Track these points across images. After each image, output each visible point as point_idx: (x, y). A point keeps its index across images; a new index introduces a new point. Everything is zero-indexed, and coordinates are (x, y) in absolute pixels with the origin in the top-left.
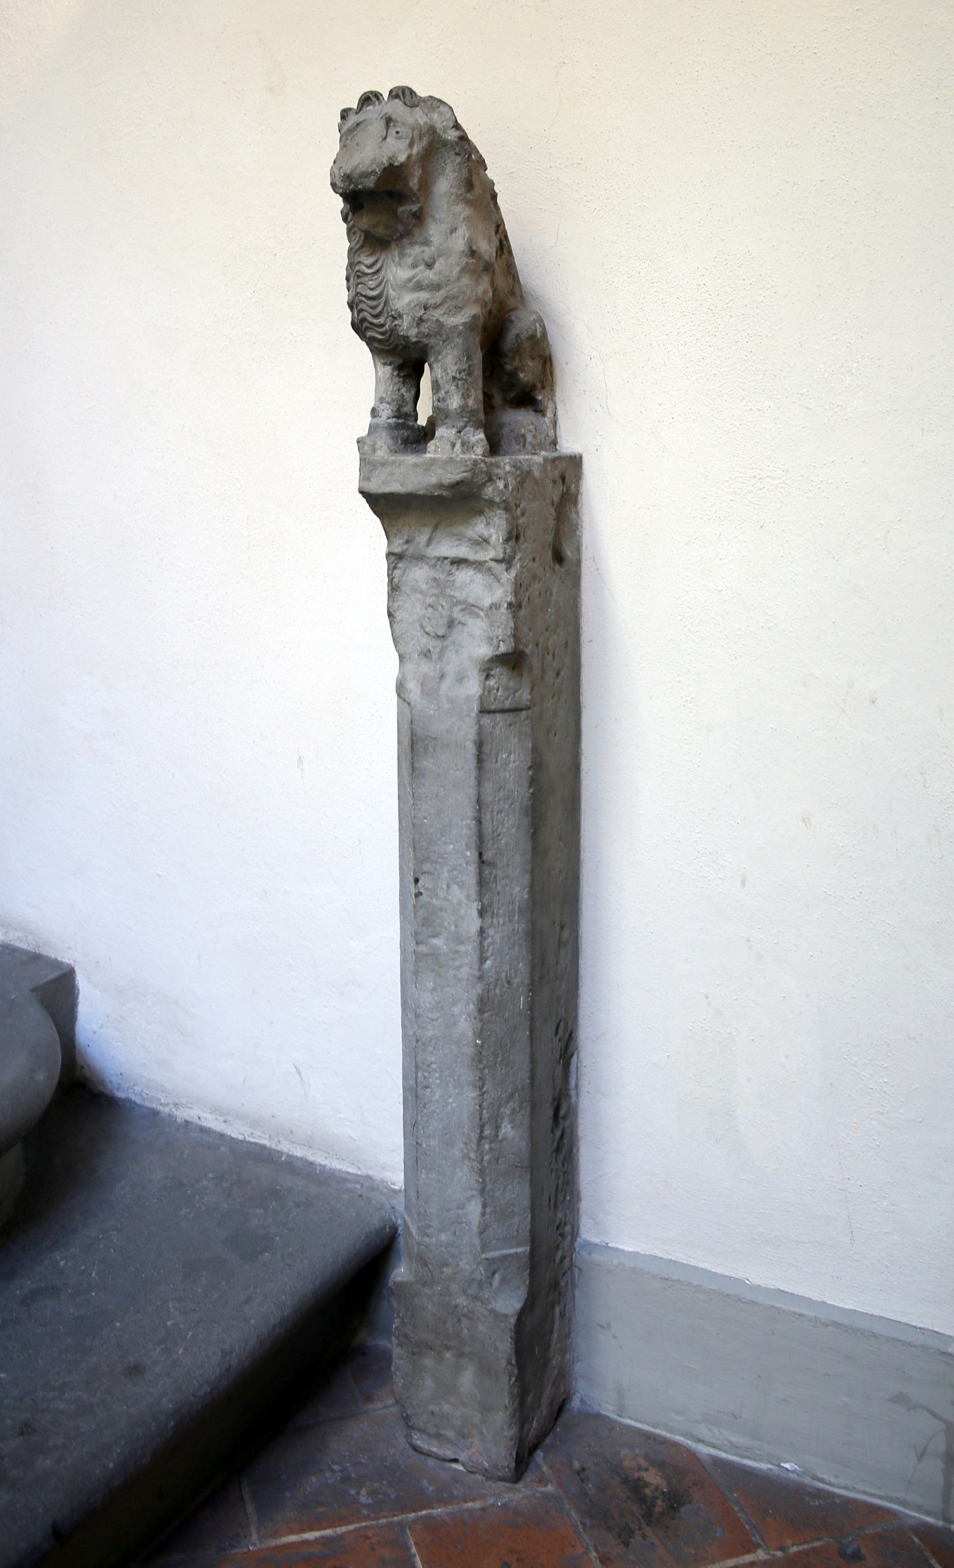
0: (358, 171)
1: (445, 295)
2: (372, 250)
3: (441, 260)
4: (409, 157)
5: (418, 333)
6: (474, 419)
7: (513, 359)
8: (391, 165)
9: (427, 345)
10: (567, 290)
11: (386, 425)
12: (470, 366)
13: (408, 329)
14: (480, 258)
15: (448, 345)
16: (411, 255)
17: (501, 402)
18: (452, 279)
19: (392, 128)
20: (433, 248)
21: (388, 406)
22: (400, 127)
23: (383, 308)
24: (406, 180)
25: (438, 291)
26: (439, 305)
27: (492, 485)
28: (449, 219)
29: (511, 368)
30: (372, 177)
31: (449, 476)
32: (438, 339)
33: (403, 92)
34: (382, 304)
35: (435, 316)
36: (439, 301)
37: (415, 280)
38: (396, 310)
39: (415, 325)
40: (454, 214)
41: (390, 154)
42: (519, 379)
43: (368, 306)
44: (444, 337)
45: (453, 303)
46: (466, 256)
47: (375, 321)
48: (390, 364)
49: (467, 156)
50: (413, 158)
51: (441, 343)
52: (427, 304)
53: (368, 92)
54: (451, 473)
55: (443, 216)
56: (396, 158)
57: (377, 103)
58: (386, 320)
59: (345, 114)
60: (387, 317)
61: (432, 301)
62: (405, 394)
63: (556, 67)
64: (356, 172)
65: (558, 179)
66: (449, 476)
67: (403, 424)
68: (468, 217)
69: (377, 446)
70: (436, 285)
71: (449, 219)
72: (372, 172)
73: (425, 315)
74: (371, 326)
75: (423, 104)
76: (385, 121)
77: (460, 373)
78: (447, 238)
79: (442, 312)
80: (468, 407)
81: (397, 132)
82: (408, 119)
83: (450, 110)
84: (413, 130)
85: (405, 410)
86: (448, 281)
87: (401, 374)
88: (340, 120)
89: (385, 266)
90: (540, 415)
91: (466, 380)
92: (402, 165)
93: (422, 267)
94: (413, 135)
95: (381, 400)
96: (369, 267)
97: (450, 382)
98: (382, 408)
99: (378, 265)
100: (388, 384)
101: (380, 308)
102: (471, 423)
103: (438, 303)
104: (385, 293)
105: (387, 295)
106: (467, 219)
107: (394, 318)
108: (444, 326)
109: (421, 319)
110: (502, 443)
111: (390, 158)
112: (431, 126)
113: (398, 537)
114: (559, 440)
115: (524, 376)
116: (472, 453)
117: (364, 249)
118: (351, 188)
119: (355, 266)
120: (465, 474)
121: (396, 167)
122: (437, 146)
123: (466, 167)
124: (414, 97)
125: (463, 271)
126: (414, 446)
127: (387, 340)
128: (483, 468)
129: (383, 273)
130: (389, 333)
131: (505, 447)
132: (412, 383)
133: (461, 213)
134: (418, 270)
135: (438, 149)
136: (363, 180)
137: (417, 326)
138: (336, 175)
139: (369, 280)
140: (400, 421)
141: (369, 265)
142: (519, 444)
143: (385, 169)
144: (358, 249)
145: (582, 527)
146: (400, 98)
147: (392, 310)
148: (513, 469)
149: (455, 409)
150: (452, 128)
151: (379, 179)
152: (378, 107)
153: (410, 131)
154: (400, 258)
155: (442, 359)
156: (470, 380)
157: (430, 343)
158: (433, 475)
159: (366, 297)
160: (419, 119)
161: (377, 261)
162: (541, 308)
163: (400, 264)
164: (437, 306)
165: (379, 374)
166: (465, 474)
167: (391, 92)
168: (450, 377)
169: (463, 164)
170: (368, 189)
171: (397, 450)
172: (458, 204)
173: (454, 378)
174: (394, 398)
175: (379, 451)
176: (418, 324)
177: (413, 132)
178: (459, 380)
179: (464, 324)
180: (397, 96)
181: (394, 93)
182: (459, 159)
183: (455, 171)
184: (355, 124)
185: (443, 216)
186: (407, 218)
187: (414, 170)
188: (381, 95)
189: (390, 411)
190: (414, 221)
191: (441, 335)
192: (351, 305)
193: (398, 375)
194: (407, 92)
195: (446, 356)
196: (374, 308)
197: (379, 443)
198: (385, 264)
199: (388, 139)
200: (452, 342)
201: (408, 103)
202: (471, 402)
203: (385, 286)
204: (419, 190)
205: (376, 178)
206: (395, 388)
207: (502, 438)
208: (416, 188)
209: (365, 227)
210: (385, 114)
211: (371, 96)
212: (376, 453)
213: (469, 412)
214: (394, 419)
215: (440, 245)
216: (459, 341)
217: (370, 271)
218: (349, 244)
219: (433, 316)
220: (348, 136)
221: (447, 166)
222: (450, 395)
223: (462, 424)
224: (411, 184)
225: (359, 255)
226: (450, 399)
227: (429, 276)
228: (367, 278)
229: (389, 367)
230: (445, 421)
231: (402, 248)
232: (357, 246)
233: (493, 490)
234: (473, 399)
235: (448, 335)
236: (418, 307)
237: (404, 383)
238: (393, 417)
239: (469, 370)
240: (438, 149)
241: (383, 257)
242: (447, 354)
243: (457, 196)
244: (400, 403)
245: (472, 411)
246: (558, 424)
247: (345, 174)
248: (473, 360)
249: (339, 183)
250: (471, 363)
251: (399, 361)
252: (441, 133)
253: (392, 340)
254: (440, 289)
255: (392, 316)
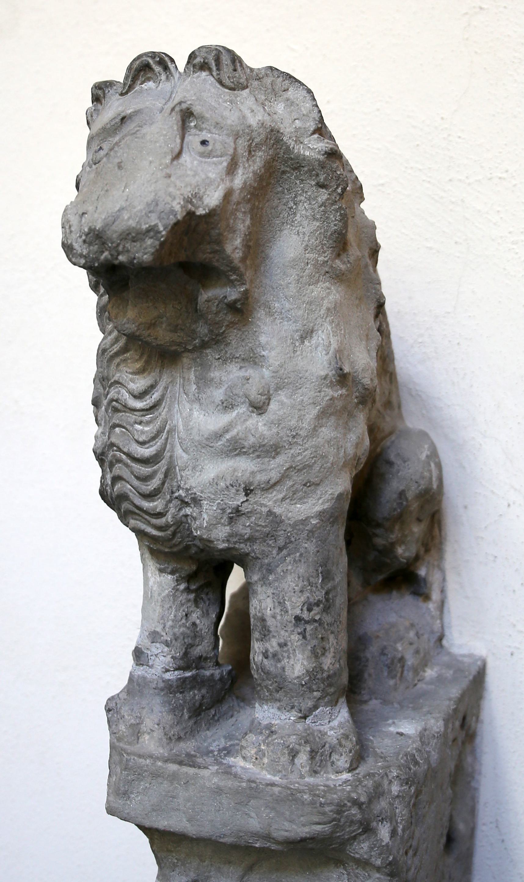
0: (119, 227)
1: (287, 465)
2: (145, 358)
3: (282, 396)
4: (228, 195)
5: (231, 535)
6: (332, 690)
7: (390, 530)
8: (190, 214)
9: (247, 554)
10: (472, 386)
11: (161, 685)
12: (327, 593)
13: (211, 526)
14: (356, 382)
15: (289, 555)
16: (221, 383)
17: (360, 588)
18: (303, 433)
19: (193, 131)
20: (266, 373)
21: (166, 649)
22: (210, 132)
23: (163, 483)
24: (219, 241)
25: (274, 458)
26: (275, 484)
27: (368, 838)
28: (300, 313)
29: (384, 542)
30: (149, 242)
31: (287, 825)
32: (270, 546)
33: (218, 60)
34: (160, 476)
35: (266, 506)
36: (274, 476)
37: (228, 436)
38: (187, 490)
39: (225, 520)
40: (310, 303)
41: (187, 192)
42: (396, 557)
43: (132, 473)
44: (281, 542)
45: (298, 478)
46: (331, 385)
47: (146, 504)
48: (172, 573)
49: (339, 190)
50: (236, 197)
51: (274, 552)
52: (251, 484)
53: (146, 54)
54: (291, 821)
55: (287, 306)
56: (201, 199)
57: (163, 77)
58: (166, 505)
59: (100, 92)
60: (170, 501)
61: (261, 478)
62: (198, 622)
63: (466, 14)
64: (114, 228)
65: (463, 201)
66: (287, 825)
67: (194, 678)
68: (335, 308)
69: (143, 728)
70: (271, 446)
71: (300, 313)
72: (148, 231)
73: (246, 504)
74: (137, 511)
75: (256, 83)
76: (179, 117)
77: (309, 610)
78: (295, 352)
79: (281, 496)
80: (322, 670)
81: (204, 143)
82: (226, 113)
83: (308, 97)
84: (237, 136)
85: (198, 651)
86: (294, 437)
87: (193, 587)
88: (90, 105)
89: (167, 400)
90: (421, 599)
91: (320, 622)
92: (212, 213)
93: (242, 409)
94: (235, 149)
95: (154, 636)
96: (140, 396)
97: (290, 628)
98: (156, 651)
99: (156, 396)
100: (167, 606)
101: (155, 483)
102: (326, 699)
103: (272, 482)
104: (167, 454)
105: (171, 457)
106: (332, 311)
107: (185, 503)
108: (282, 521)
109: (237, 511)
110: (366, 675)
111: (189, 201)
112: (272, 131)
113: (177, 870)
114: (447, 633)
115: (405, 551)
116: (330, 769)
117: (128, 355)
118: (102, 257)
119: (110, 387)
120: (319, 828)
121: (201, 216)
122: (283, 168)
123: (336, 211)
124: (239, 68)
125: (323, 414)
126: (213, 712)
127: (170, 540)
128: (354, 815)
129: (163, 411)
130: (172, 529)
131: (370, 683)
132: (211, 596)
133: (323, 299)
134: (234, 414)
135: (284, 172)
136: (128, 245)
137: (229, 524)
138: (73, 229)
139: (136, 423)
140: (188, 674)
141: (136, 393)
142: (394, 677)
143: (177, 224)
144: (117, 354)
145: (480, 773)
146: (210, 70)
147: (179, 487)
148: (405, 787)
149: (298, 677)
150: (314, 133)
151: (162, 244)
152: (165, 86)
153: (230, 141)
154: (198, 388)
155: (275, 580)
156: (327, 619)
157: (253, 551)
158: (253, 814)
159: (128, 455)
160: (249, 114)
161: (152, 387)
162: (424, 412)
163: (198, 400)
164: (269, 487)
165: (151, 583)
166: (319, 828)
167: (192, 56)
168: (289, 617)
169: (332, 204)
170: (140, 264)
171: (182, 735)
172: (318, 282)
173: (298, 619)
174: (178, 634)
175: (147, 737)
176: (231, 520)
177: (235, 142)
178: (307, 622)
179: (320, 514)
180: (204, 66)
181: (198, 60)
182: (323, 195)
183: (315, 219)
184: (118, 120)
185: (287, 306)
186: (217, 313)
187: (236, 219)
188: (172, 61)
189: (169, 658)
190: (230, 317)
191: (275, 538)
192: (100, 457)
193: (188, 590)
194: (225, 60)
195: (283, 577)
196: (145, 479)
197: (149, 723)
198: (168, 395)
199: (185, 157)
200: (297, 549)
201: (227, 82)
202: (328, 662)
203: (167, 439)
204: (243, 260)
205: (157, 243)
206: (181, 614)
207: (366, 666)
208: (237, 255)
209: (132, 328)
210: (180, 103)
211: (151, 61)
212: (141, 740)
213: (323, 680)
214: (176, 672)
215: (281, 366)
216: (310, 546)
217: (139, 405)
218: (101, 336)
219: (262, 505)
220: (104, 140)
221: (300, 207)
222: (288, 650)
223: (310, 704)
224: (229, 249)
225: (118, 365)
226: (289, 657)
227: (257, 429)
228: (132, 417)
229: (170, 577)
230: (278, 696)
231: (205, 367)
232: (116, 348)
233: (371, 849)
234: (332, 654)
235: (288, 537)
236: (233, 490)
237: (196, 602)
238: (176, 669)
239: (327, 600)
240: (284, 172)
241: (165, 380)
242: (285, 572)
243: (317, 266)
244: (188, 641)
245: (329, 677)
246: (446, 605)
247: (91, 230)
248: (333, 579)
249: (78, 247)
250: (329, 585)
251: (190, 568)
252: (292, 143)
253: (177, 539)
254: (277, 454)
255: (179, 498)
